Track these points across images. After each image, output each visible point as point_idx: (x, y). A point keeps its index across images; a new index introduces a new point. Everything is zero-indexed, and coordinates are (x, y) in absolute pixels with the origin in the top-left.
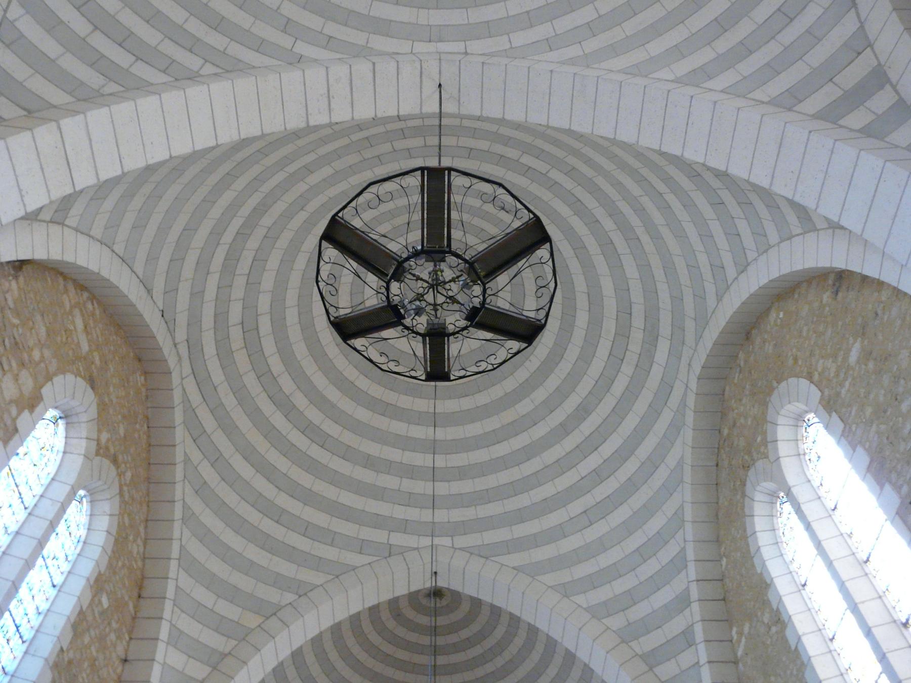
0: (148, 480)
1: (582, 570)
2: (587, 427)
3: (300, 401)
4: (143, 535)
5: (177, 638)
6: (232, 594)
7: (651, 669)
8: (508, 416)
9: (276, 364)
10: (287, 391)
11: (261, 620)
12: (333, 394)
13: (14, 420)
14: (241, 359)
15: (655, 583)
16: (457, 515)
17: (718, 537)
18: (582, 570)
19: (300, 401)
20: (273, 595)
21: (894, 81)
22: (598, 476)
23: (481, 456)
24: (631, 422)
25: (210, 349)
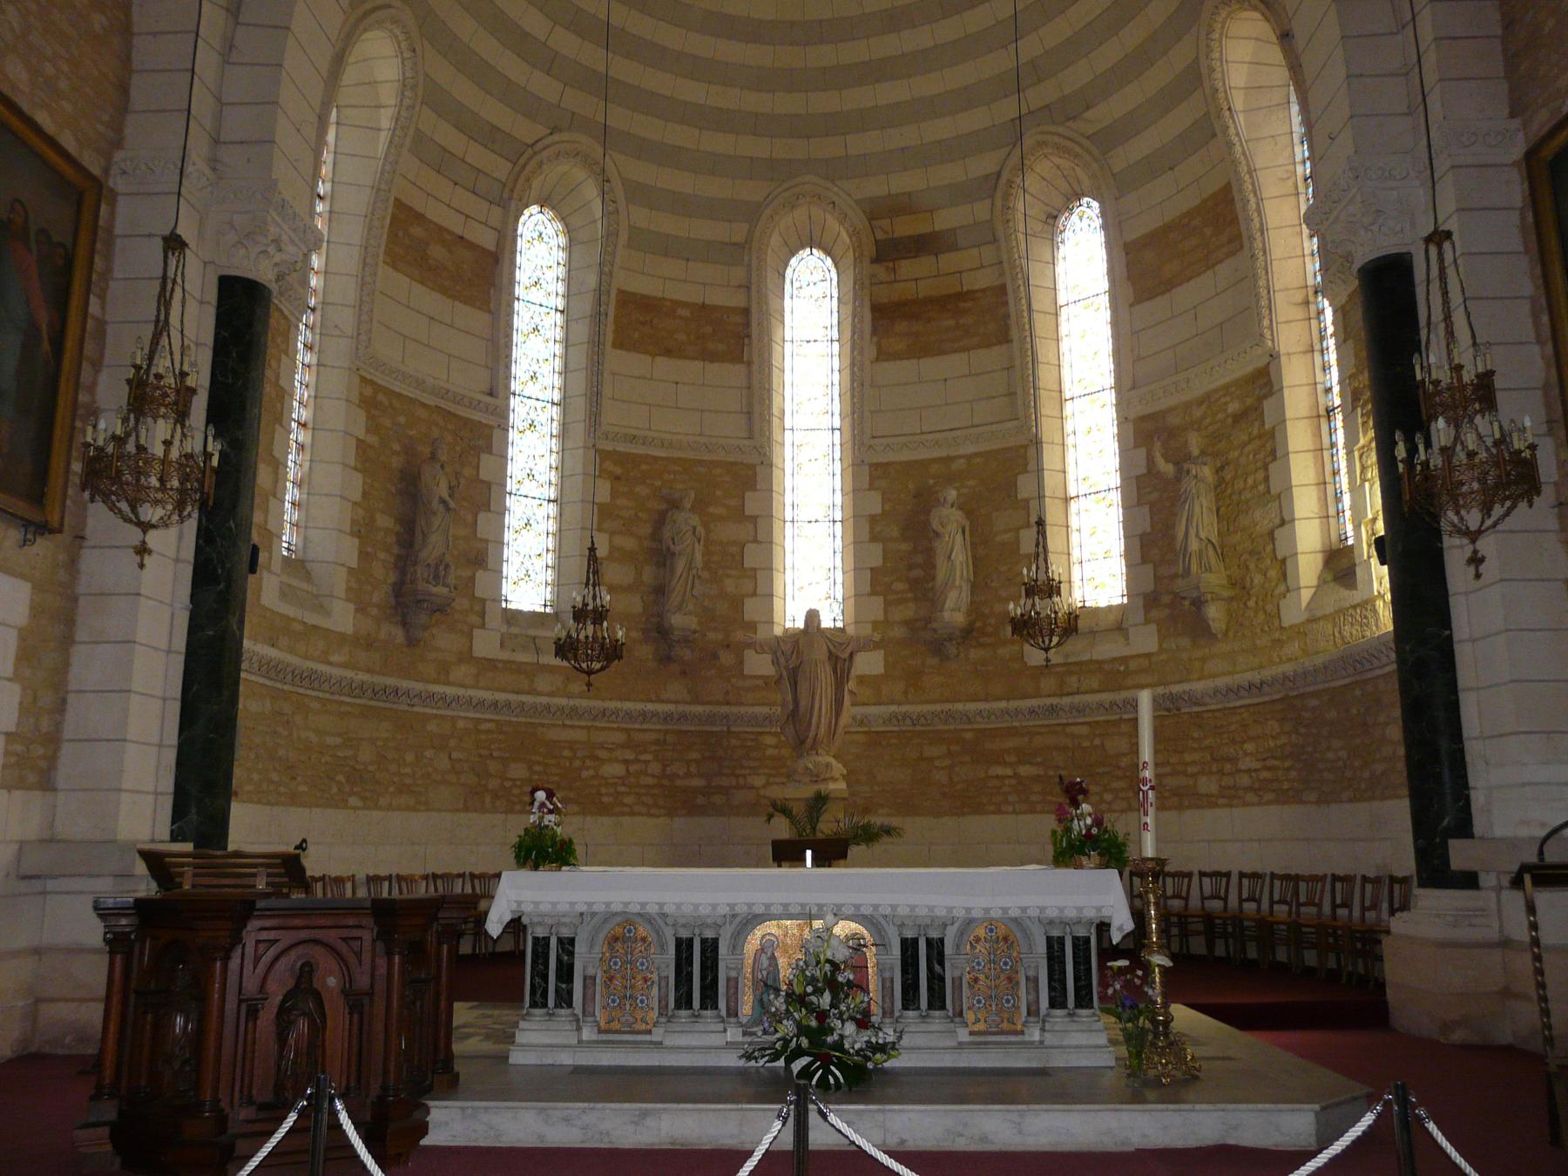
24: (512, 67)
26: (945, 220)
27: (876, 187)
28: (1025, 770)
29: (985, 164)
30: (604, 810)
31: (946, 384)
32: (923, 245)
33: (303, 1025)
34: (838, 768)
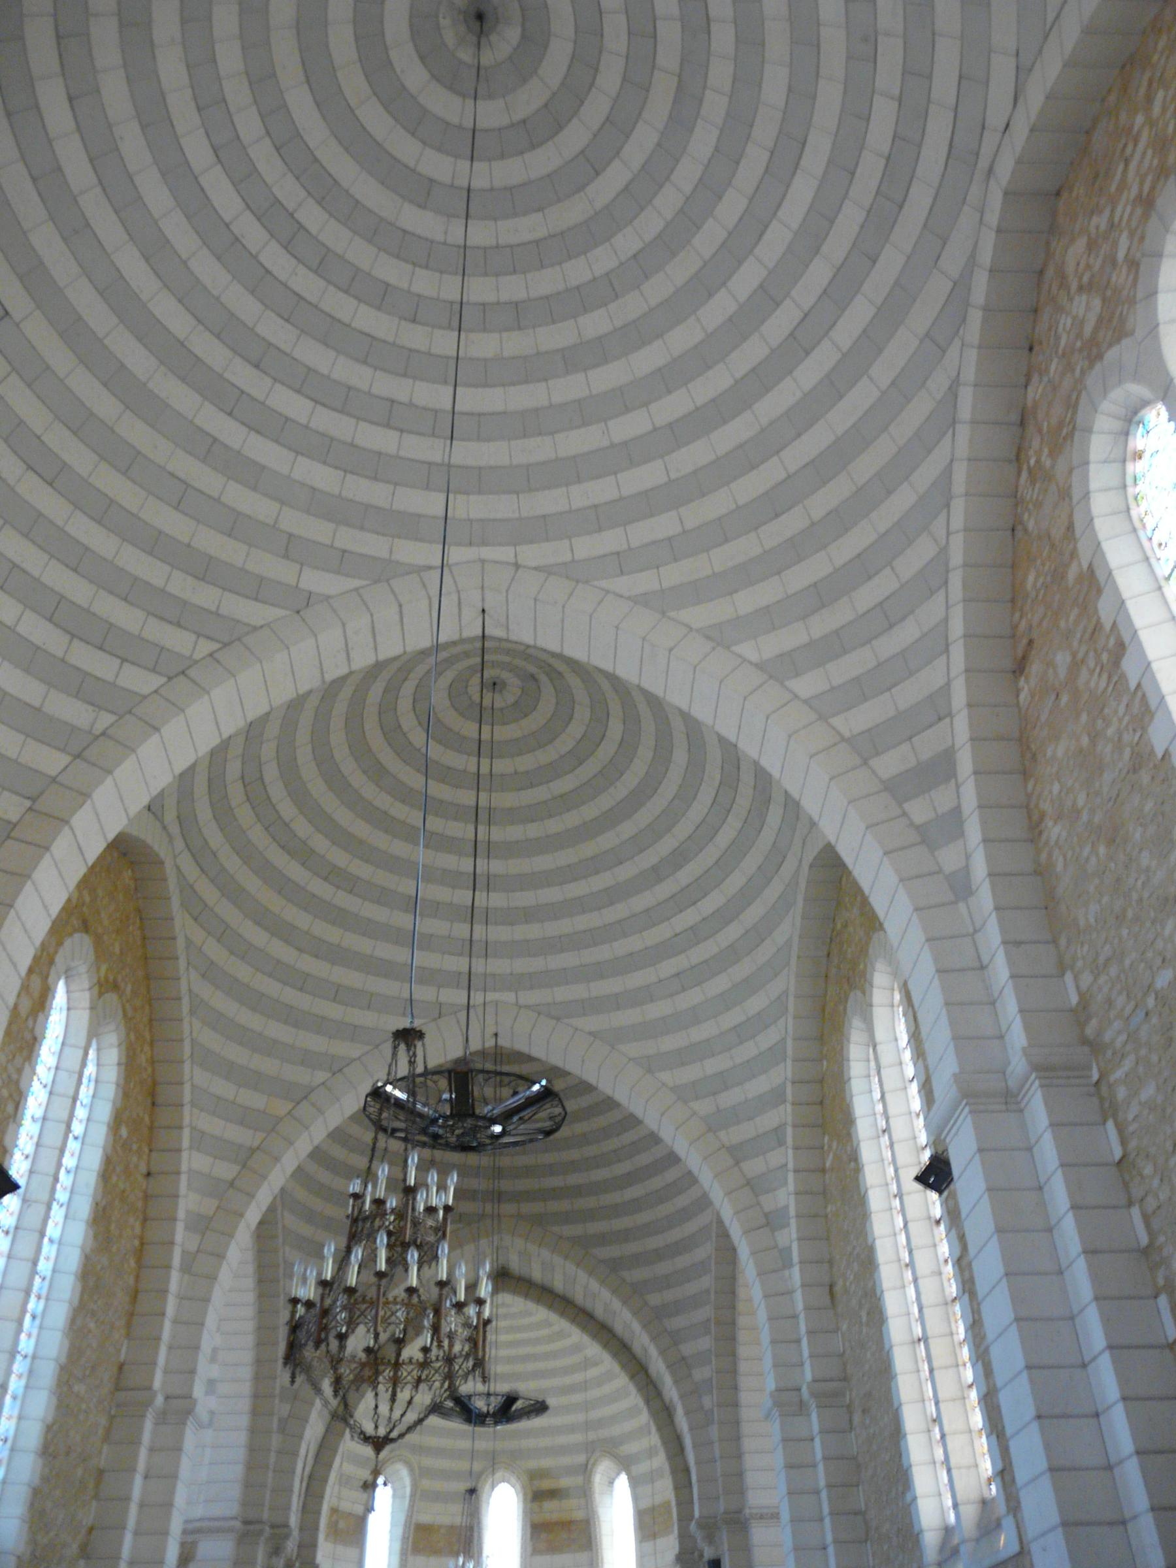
0: (147, 977)
1: (670, 1043)
2: (685, 876)
3: (320, 843)
4: (148, 1036)
5: (201, 1140)
7: (737, 1163)
9: (287, 809)
10: (301, 834)
11: (290, 1106)
12: (361, 829)
13: (32, 1030)
14: (245, 815)
16: (523, 965)
17: (822, 1035)
18: (670, 1043)
19: (320, 843)
21: (960, 780)
22: (695, 935)
24: (736, 881)
26: (565, 1482)
27: (533, 1464)
29: (581, 1459)
32: (553, 1494)
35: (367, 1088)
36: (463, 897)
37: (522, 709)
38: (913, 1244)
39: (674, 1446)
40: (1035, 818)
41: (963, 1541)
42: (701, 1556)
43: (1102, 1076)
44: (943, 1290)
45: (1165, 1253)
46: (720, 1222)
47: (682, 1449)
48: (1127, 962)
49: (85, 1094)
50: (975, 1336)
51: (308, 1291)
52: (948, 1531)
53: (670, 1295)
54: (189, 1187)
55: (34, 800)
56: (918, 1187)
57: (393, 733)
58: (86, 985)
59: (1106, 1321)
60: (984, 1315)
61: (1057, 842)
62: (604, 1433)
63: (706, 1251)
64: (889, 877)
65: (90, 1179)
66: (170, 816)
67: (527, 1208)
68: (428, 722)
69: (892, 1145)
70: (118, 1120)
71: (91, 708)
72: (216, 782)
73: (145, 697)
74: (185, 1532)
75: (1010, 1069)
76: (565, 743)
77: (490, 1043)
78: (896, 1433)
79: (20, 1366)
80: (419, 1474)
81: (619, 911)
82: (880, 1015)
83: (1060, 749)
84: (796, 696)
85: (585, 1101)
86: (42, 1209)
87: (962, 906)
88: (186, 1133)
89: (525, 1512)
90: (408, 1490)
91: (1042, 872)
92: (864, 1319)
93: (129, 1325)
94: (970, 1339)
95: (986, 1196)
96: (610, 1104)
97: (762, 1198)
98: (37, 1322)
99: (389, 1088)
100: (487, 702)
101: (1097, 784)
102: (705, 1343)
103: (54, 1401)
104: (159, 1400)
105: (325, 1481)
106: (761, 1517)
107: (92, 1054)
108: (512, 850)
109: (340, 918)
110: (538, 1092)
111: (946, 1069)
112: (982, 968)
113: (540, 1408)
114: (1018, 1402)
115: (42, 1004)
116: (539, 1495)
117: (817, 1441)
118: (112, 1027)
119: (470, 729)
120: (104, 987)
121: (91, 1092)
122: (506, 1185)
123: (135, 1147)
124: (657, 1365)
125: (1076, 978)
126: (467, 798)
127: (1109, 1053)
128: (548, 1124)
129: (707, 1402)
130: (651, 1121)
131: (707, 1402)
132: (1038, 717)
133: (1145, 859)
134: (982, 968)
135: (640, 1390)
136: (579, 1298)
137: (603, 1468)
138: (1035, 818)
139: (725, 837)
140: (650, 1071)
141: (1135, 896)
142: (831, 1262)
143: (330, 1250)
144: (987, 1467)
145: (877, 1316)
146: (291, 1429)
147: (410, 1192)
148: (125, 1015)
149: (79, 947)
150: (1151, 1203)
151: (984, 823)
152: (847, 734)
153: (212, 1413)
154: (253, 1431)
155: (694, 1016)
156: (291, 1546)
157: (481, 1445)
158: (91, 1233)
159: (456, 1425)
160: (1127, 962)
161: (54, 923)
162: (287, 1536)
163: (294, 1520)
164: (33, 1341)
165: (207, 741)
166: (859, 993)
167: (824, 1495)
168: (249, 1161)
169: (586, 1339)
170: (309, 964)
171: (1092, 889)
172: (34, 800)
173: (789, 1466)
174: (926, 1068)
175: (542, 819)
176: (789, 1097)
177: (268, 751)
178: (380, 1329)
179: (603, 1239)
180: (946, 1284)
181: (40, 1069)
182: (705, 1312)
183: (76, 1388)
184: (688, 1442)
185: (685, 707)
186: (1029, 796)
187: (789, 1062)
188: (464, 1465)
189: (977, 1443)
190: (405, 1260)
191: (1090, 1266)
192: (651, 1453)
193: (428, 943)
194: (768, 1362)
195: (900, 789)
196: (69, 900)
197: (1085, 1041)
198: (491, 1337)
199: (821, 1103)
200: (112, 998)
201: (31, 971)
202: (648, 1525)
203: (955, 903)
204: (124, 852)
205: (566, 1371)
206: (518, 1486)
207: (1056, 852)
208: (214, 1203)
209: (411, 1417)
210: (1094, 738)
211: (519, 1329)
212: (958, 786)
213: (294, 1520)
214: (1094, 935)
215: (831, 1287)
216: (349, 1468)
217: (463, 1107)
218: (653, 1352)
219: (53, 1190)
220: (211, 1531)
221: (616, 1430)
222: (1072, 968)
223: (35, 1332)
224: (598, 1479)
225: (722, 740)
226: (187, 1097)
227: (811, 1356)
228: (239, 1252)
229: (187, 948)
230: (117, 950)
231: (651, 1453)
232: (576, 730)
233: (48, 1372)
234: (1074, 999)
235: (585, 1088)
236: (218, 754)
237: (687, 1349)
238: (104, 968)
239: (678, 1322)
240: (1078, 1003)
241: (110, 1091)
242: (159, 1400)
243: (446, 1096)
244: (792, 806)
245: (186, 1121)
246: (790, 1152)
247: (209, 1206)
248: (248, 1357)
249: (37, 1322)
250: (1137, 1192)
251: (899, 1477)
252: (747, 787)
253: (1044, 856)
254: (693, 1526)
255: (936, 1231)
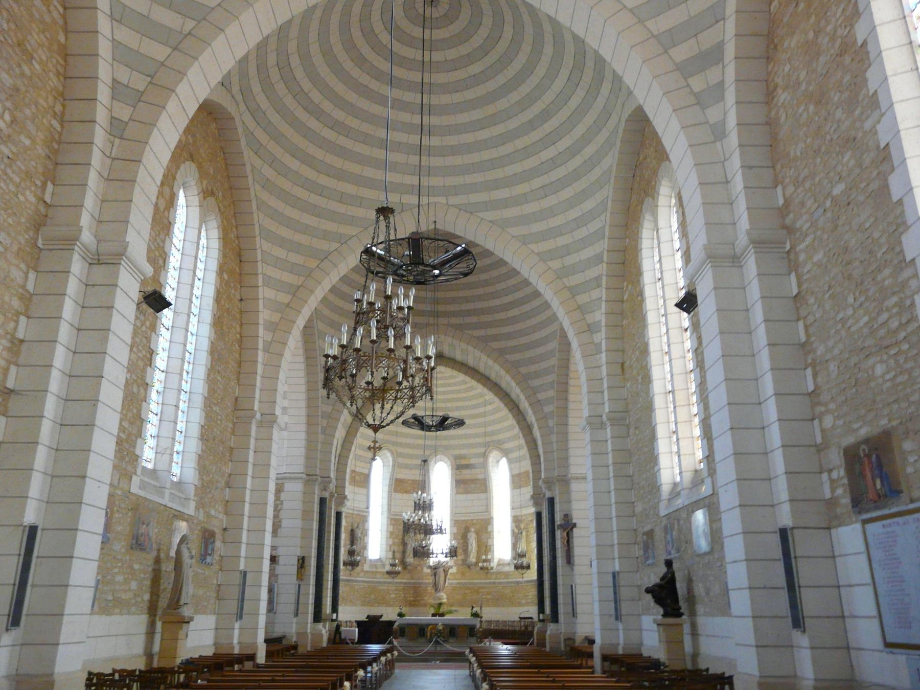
0: (231, 188)
1: (537, 227)
2: (549, 127)
3: (327, 106)
6: (297, 248)
7: (573, 297)
8: (490, 110)
9: (306, 85)
10: (316, 101)
12: (352, 97)
13: (168, 218)
14: (280, 88)
15: (584, 243)
16: (451, 181)
18: (537, 227)
19: (327, 106)
20: (324, 246)
21: (725, 63)
22: (554, 163)
23: (468, 138)
24: (580, 130)
25: (256, 88)
26: (473, 461)
27: (457, 452)
28: (489, 597)
30: (391, 606)
31: (472, 501)
32: (467, 466)
33: (857, 466)
34: (445, 596)
35: (362, 249)
36: (415, 139)
37: (450, 18)
38: (671, 341)
39: (532, 444)
40: (771, 88)
41: (683, 489)
42: (544, 496)
43: (793, 247)
44: (685, 366)
45: (814, 346)
46: (562, 329)
47: (536, 445)
48: (817, 179)
49: (202, 255)
50: (701, 390)
51: (334, 351)
52: (675, 485)
53: (533, 368)
54: (264, 307)
55: (152, 77)
56: (677, 310)
57: (369, 34)
58: (196, 193)
59: (775, 381)
60: (708, 378)
61: (783, 104)
62: (496, 438)
63: (553, 345)
64: (675, 125)
65: (209, 302)
66: (236, 89)
67: (454, 321)
68: (391, 27)
69: (663, 287)
70: (221, 270)
71: (180, 16)
72: (262, 68)
73: (213, 9)
74: (277, 479)
75: (737, 242)
76: (477, 41)
77: (432, 227)
78: (653, 438)
79: (184, 397)
80: (396, 456)
81: (508, 149)
82: (662, 212)
83: (793, 42)
84: (625, 7)
85: (487, 261)
86: (185, 317)
87: (718, 144)
88: (260, 277)
89: (452, 474)
90: (391, 463)
91: (771, 124)
92: (640, 380)
93: (238, 380)
94: (698, 392)
95: (716, 314)
96: (501, 263)
97: (587, 316)
98: (190, 376)
99: (374, 249)
100: (428, 14)
101: (815, 64)
102: (551, 393)
103: (204, 414)
104: (258, 416)
105: (348, 457)
106: (577, 478)
107: (203, 233)
108: (444, 110)
109: (341, 152)
110: (461, 251)
111: (699, 242)
112: (727, 182)
113: (460, 423)
114: (721, 421)
115: (171, 202)
116: (460, 466)
117: (609, 442)
118: (213, 217)
119: (417, 32)
120: (206, 193)
121: (205, 254)
122: (441, 308)
123: (232, 285)
124: (525, 405)
125: (784, 189)
126: (416, 77)
127: (798, 235)
128: (465, 270)
129: (551, 423)
130: (525, 273)
131: (551, 423)
132: (782, 20)
133: (839, 114)
134: (727, 182)
135: (514, 416)
136: (482, 369)
137: (493, 455)
138: (771, 88)
139: (574, 102)
140: (524, 244)
141: (828, 137)
142: (623, 351)
143: (345, 329)
144: (700, 455)
145: (647, 379)
146: (329, 432)
147: (388, 298)
148: (220, 210)
149: (188, 171)
150: (811, 319)
151: (737, 91)
152: (656, 33)
153: (286, 423)
154: (308, 433)
155: (552, 212)
156: (332, 486)
157: (429, 442)
158: (213, 331)
159: (418, 432)
160: (817, 179)
161: (173, 153)
162: (330, 482)
163: (332, 475)
164: (189, 385)
165: (254, 38)
166: (650, 199)
167: (611, 468)
168: (297, 293)
169: (486, 391)
170: (323, 180)
171: (801, 133)
172: (152, 77)
173: (593, 454)
174: (688, 243)
175: (462, 91)
176: (605, 259)
177: (292, 46)
178: (374, 370)
179: (495, 338)
180: (687, 363)
181: (175, 240)
182: (553, 361)
183: (214, 408)
184: (540, 443)
185: (552, 14)
186: (769, 74)
187: (606, 240)
188: (420, 452)
189: (696, 443)
190: (387, 335)
191: (770, 352)
192: (520, 448)
193: (395, 167)
194: (585, 402)
195: (686, 69)
196: (180, 141)
197: (784, 227)
198: (435, 375)
199: (624, 263)
200: (211, 200)
201: (162, 184)
202: (517, 481)
203: (714, 142)
204: (209, 112)
205: (474, 407)
206: (449, 463)
207: (782, 110)
208: (279, 315)
209: (391, 417)
210: (817, 33)
211: (449, 385)
212: (724, 67)
213: (332, 475)
214: (798, 163)
215: (623, 364)
216: (360, 452)
217: (417, 259)
218: (522, 397)
219: (190, 307)
220: (290, 478)
221: (501, 437)
222: (782, 183)
223: (189, 380)
224: (491, 459)
225: (576, 37)
226: (259, 257)
227: (609, 400)
228: (294, 341)
229: (252, 170)
230: (212, 172)
231: (520, 448)
232: (483, 32)
233: (199, 400)
234: (781, 202)
235: (488, 253)
236: (262, 46)
237: (541, 396)
238: (205, 182)
239: (536, 383)
240: (783, 205)
241: (215, 253)
242: (258, 416)
243: (407, 253)
244: (617, 80)
245: (260, 271)
246: (604, 290)
247: (276, 317)
248: (303, 396)
249: (190, 376)
250: (803, 313)
251: (652, 459)
252: (591, 68)
253: (773, 113)
254: (540, 482)
255: (684, 334)
